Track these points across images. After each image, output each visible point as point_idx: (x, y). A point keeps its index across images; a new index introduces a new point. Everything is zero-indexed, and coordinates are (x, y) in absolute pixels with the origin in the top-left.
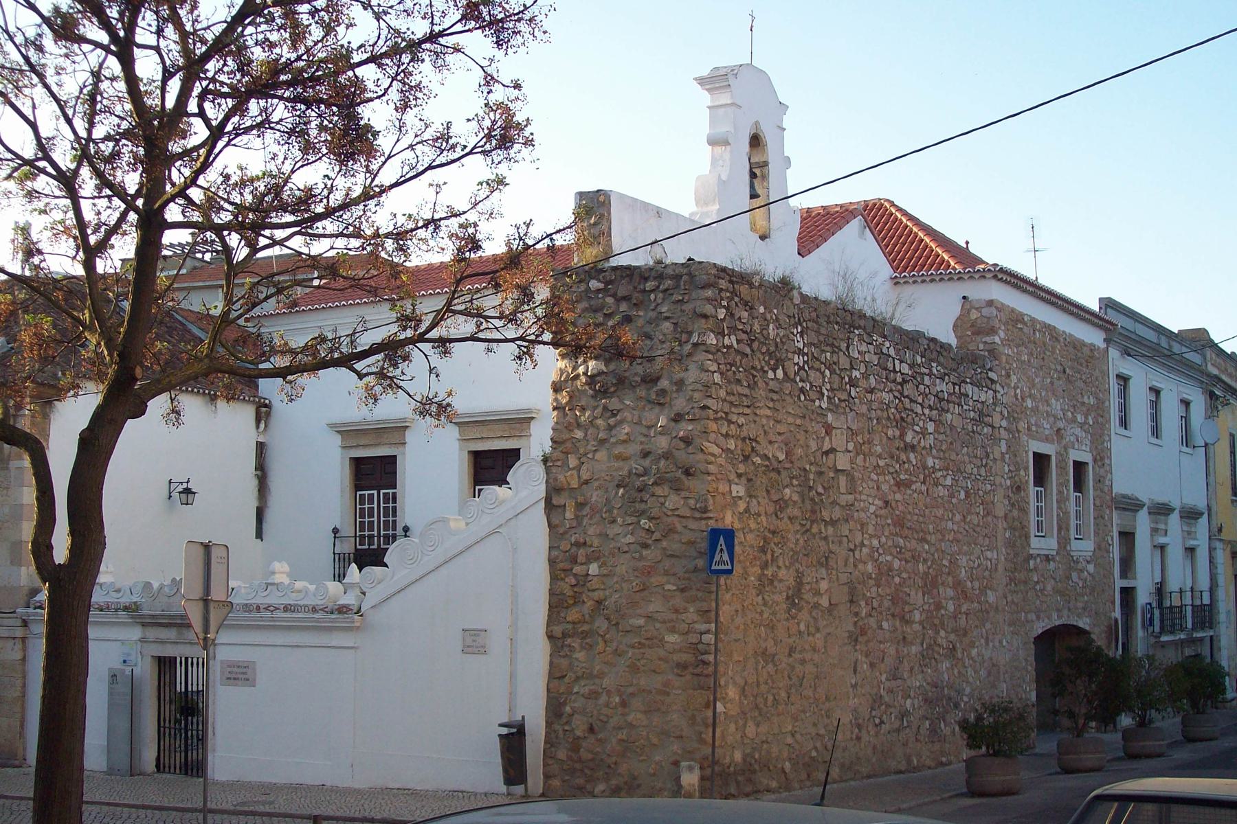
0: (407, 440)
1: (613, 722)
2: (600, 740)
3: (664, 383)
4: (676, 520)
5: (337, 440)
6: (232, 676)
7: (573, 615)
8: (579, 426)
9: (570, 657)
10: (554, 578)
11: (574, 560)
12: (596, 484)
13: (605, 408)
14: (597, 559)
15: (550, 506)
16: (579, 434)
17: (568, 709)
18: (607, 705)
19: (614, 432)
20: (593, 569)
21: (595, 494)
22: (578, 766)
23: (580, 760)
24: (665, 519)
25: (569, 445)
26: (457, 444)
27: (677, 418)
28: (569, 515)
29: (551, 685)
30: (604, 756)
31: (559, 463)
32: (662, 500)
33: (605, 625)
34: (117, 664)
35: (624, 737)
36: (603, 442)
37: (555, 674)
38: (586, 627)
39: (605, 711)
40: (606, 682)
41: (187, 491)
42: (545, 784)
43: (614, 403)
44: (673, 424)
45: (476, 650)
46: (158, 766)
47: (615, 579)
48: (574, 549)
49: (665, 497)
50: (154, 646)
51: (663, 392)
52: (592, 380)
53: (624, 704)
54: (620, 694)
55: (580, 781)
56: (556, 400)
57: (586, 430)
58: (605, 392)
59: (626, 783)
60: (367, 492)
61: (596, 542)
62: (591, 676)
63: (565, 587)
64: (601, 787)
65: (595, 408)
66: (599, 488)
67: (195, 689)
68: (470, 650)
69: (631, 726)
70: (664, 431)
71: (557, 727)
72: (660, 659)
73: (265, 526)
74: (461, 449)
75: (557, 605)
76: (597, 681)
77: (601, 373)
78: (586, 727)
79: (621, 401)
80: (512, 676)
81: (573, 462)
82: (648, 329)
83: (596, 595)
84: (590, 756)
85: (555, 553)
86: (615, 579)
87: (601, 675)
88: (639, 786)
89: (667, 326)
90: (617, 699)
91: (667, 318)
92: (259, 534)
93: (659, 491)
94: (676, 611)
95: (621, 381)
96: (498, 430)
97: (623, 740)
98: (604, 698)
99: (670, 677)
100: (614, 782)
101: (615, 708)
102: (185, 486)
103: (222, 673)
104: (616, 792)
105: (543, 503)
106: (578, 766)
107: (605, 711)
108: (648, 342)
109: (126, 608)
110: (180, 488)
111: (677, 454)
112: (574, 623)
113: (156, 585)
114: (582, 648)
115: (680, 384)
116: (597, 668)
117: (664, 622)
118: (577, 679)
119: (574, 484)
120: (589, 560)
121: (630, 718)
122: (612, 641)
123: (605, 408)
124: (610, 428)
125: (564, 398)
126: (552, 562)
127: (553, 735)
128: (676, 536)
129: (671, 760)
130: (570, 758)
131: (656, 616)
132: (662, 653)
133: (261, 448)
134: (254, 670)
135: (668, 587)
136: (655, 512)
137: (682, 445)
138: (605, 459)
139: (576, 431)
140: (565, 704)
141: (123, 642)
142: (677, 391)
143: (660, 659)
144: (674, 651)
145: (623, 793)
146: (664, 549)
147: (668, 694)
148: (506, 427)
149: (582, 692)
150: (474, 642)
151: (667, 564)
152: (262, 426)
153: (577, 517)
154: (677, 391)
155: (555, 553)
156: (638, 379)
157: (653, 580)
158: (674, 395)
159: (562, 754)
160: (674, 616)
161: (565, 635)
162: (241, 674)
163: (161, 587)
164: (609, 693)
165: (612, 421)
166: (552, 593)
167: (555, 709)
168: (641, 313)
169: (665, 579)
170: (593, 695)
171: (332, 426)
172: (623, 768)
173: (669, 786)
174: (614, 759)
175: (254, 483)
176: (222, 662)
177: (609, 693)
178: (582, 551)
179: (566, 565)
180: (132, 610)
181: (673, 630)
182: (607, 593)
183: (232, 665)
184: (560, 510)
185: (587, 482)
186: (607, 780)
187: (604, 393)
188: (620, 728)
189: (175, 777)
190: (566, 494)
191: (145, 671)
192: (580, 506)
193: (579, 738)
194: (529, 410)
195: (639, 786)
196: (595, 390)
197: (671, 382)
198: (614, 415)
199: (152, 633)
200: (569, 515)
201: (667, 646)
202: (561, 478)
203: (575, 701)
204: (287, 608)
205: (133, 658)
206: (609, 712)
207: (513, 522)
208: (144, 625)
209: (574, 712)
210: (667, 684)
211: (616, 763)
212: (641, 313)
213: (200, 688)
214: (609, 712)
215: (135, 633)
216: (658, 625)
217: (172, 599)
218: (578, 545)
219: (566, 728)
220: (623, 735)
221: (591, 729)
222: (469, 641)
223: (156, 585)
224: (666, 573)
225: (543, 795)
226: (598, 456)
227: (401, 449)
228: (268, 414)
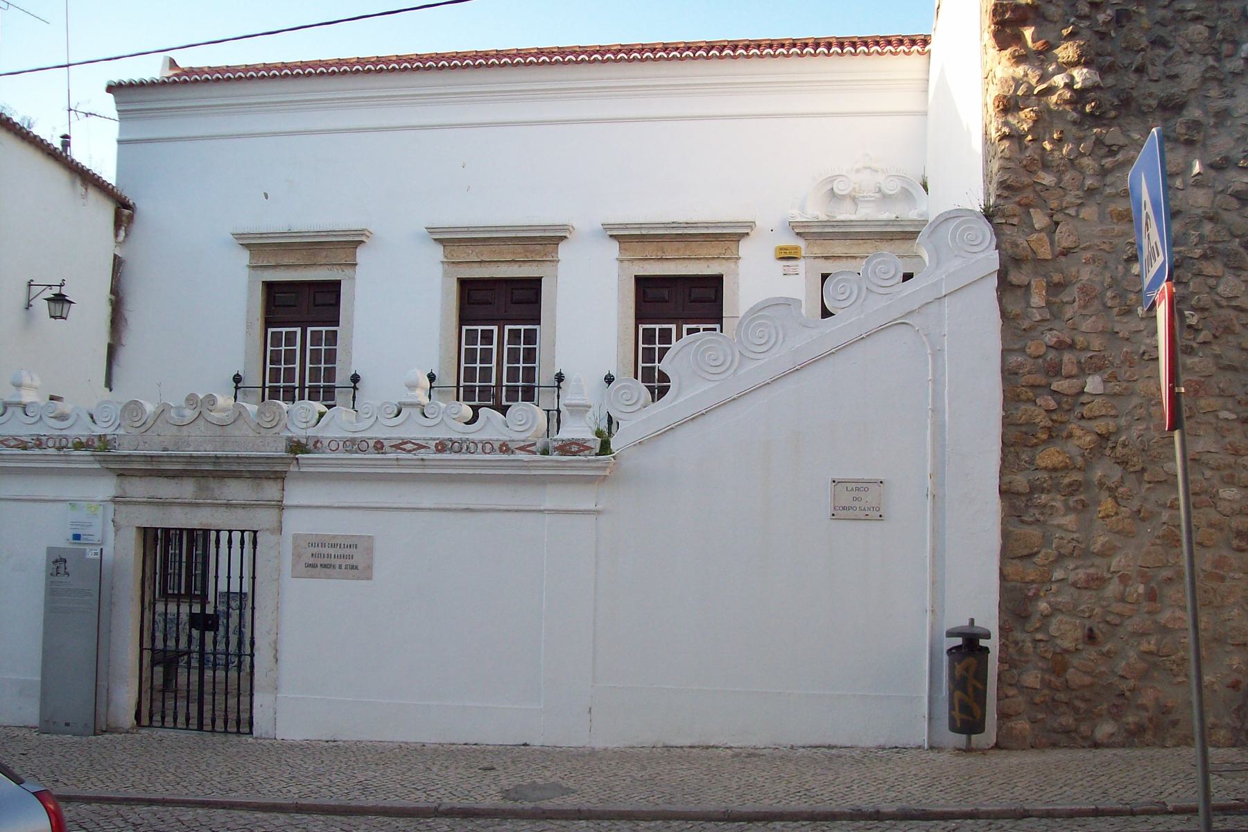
0: (358, 260)
1: (1131, 625)
2: (1107, 655)
3: (1194, 112)
4: (1233, 313)
5: (244, 257)
6: (319, 561)
7: (1049, 456)
8: (1046, 166)
9: (1044, 523)
10: (1011, 398)
11: (1055, 370)
12: (1089, 254)
13: (1099, 142)
14: (1098, 369)
15: (1005, 285)
16: (1047, 179)
17: (1043, 606)
18: (1122, 599)
19: (1109, 179)
20: (1093, 384)
21: (1088, 269)
22: (1062, 696)
23: (1067, 687)
24: (1216, 311)
25: (1029, 194)
26: (439, 270)
27: (1220, 166)
28: (1037, 300)
29: (1009, 569)
30: (1114, 679)
31: (1015, 221)
32: (1212, 282)
33: (1116, 473)
34: (61, 540)
35: (1153, 647)
36: (1091, 192)
37: (1011, 551)
38: (1076, 476)
39: (1117, 607)
40: (1117, 562)
41: (60, 299)
42: (999, 728)
43: (1113, 135)
44: (1213, 173)
45: (861, 514)
46: (138, 716)
47: (1135, 401)
48: (1052, 355)
49: (1218, 277)
50: (146, 510)
51: (1196, 125)
52: (1079, 96)
53: (1152, 596)
54: (1145, 578)
55: (1068, 720)
56: (1006, 124)
57: (1060, 174)
58: (1101, 117)
59: (1150, 720)
60: (284, 330)
61: (1096, 343)
62: (1086, 554)
63: (1037, 412)
64: (1105, 729)
65: (1079, 140)
66: (1094, 259)
67: (223, 587)
68: (850, 513)
69: (1164, 630)
70: (1199, 183)
71: (1018, 635)
72: (1211, 525)
73: (116, 370)
74: (446, 274)
75: (1017, 441)
76: (1097, 561)
77: (1095, 88)
78: (1079, 633)
79: (1125, 133)
80: (938, 556)
81: (1039, 219)
82: (1162, 32)
83: (1100, 426)
84: (1087, 680)
85: (1015, 359)
86: (1135, 401)
87: (1107, 552)
88: (1175, 723)
89: (1197, 31)
90: (1141, 589)
91: (1197, 19)
92: (109, 383)
93: (1208, 268)
94: (1236, 453)
95: (1126, 103)
96: (518, 252)
97: (1150, 653)
98: (1113, 588)
99: (1225, 553)
100: (1131, 719)
101: (1137, 602)
102: (56, 290)
103: (297, 556)
104: (1134, 736)
105: (994, 281)
106: (1062, 696)
107: (1117, 607)
108: (1162, 52)
109: (79, 446)
110: (49, 294)
111: (1226, 216)
112: (1055, 469)
113: (150, 408)
114: (1069, 510)
115: (1223, 115)
116: (1102, 540)
117: (1218, 469)
118: (1061, 557)
119: (1045, 252)
120: (1083, 370)
121: (1165, 616)
122: (1129, 497)
123: (1099, 142)
124: (1104, 172)
125: (1024, 120)
126: (1009, 374)
127: (1012, 650)
128: (1230, 338)
129: (1229, 680)
130: (1046, 684)
131: (1204, 457)
132: (1214, 516)
133: (118, 263)
134: (370, 551)
135: (1224, 414)
136: (1205, 299)
137: (1235, 204)
138: (1095, 217)
139: (1041, 174)
140: (1036, 596)
141: (72, 503)
142: (1216, 126)
143: (1211, 525)
144: (1235, 513)
145: (1148, 736)
146: (1217, 357)
147: (1222, 579)
148: (519, 249)
149: (1072, 577)
150: (856, 501)
151: (1223, 380)
152: (122, 233)
153: (1049, 304)
154: (1216, 126)
155: (1015, 359)
156: (1154, 103)
157: (1202, 403)
158: (1213, 131)
159: (1031, 678)
160: (1231, 459)
161: (1034, 488)
162: (334, 559)
163: (163, 410)
164: (1124, 579)
165: (1107, 162)
166: (1007, 422)
167: (1016, 604)
168: (1143, 11)
169: (1220, 401)
170: (1096, 583)
171: (238, 236)
172: (1147, 698)
173: (1227, 720)
174: (1132, 683)
175: (107, 310)
176: (296, 537)
177: (1124, 579)
178: (1067, 357)
179: (1040, 379)
180: (100, 447)
181: (1230, 481)
182: (1123, 422)
183: (319, 542)
184: (1019, 292)
185: (1066, 252)
186: (1116, 713)
187: (1097, 118)
188: (1144, 634)
189: (183, 734)
190: (1027, 268)
191: (122, 552)
192: (1055, 288)
193: (1067, 651)
194: (564, 227)
195: (1175, 723)
196: (1083, 113)
197: (1206, 113)
198: (1112, 153)
199: (139, 488)
200: (1037, 300)
201: (1223, 506)
202: (1022, 241)
203: (1057, 593)
204: (441, 447)
205: (95, 531)
206: (1126, 609)
207: (933, 309)
208: (121, 474)
209: (1055, 610)
210: (1219, 563)
211: (1132, 690)
212: (1143, 11)
213: (235, 588)
214: (1126, 609)
215: (106, 488)
216: (1208, 473)
217: (185, 431)
218: (1060, 346)
219: (1039, 636)
220: (1150, 644)
221: (1091, 637)
222: (846, 498)
223: (150, 408)
224: (1222, 394)
225: (997, 746)
226: (1085, 213)
227: (348, 271)
228: (131, 218)
